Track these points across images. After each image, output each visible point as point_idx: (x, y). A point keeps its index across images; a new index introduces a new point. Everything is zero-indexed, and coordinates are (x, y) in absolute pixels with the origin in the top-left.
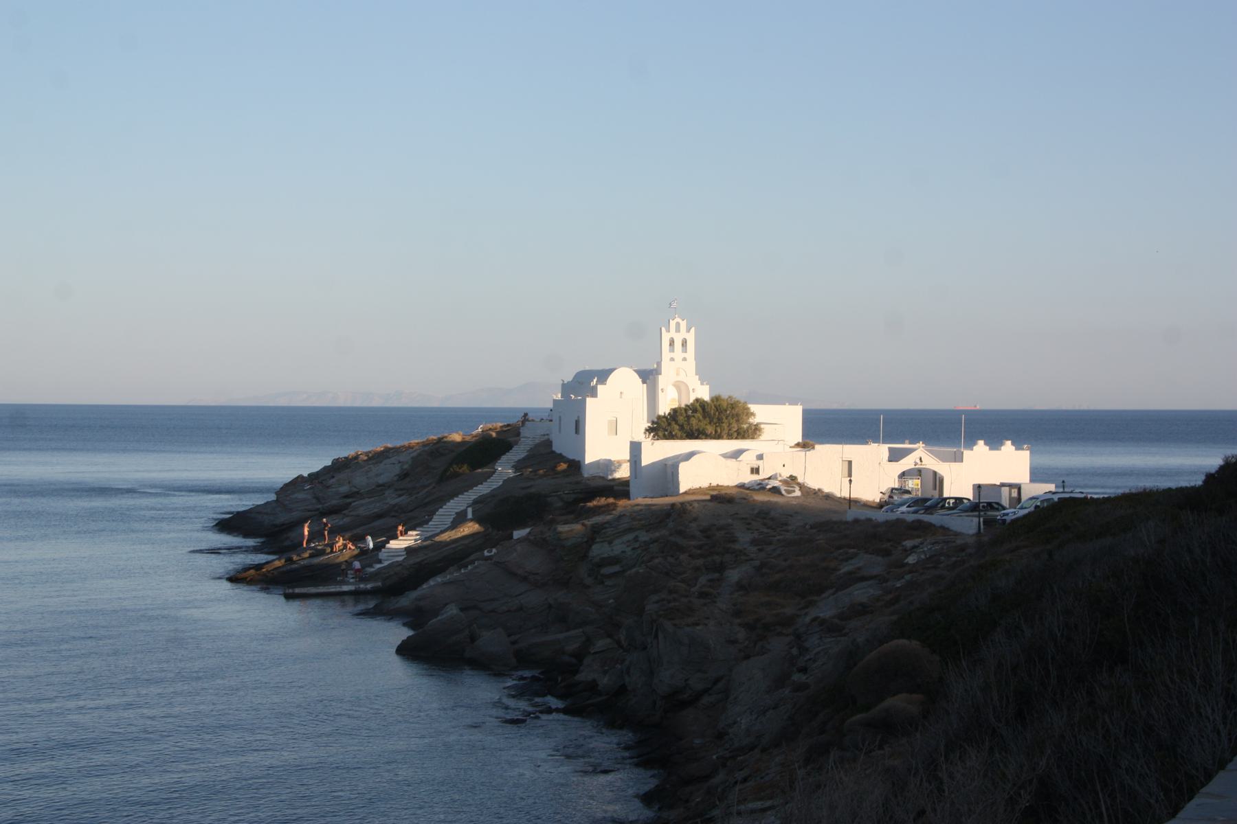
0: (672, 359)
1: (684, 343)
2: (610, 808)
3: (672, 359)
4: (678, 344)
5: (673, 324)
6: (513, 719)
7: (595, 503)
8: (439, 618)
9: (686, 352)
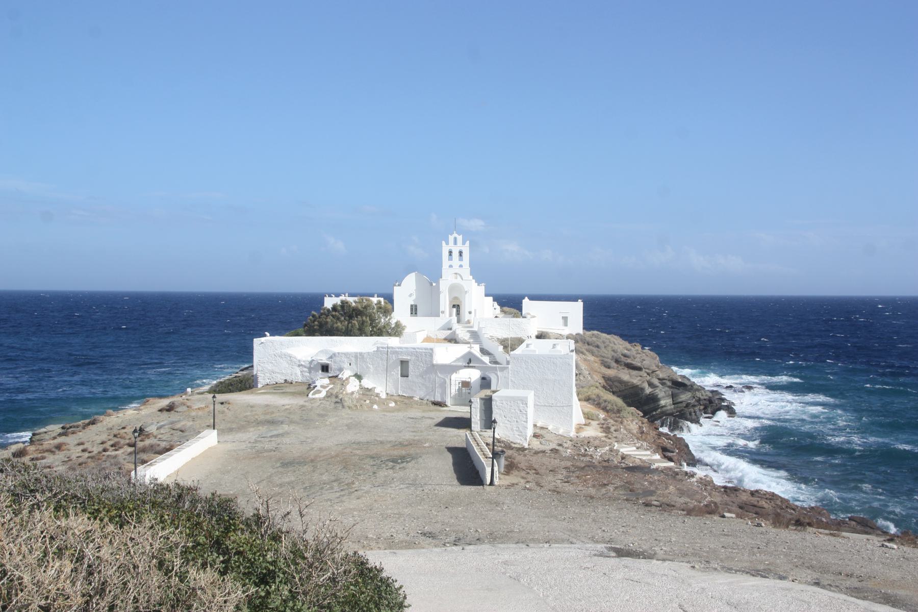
0: (451, 266)
1: (461, 253)
2: (43, 430)
4: (455, 254)
5: (451, 238)
6: (114, 411)
7: (686, 372)
8: (880, 440)
9: (452, 260)
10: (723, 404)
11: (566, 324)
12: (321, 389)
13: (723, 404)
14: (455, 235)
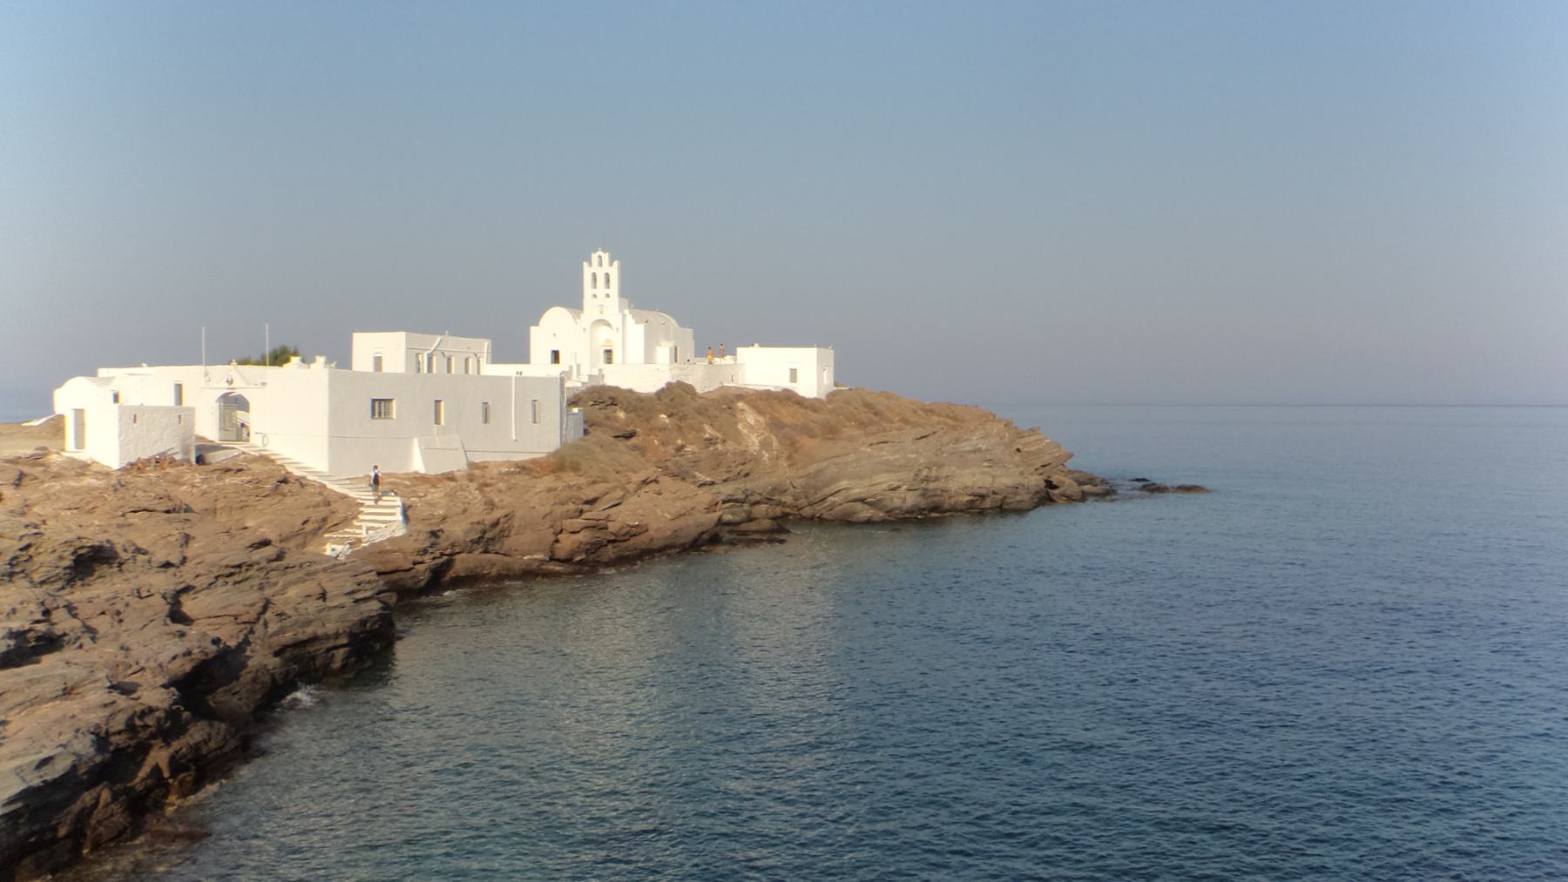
3: (595, 296)
5: (595, 257)
14: (600, 253)
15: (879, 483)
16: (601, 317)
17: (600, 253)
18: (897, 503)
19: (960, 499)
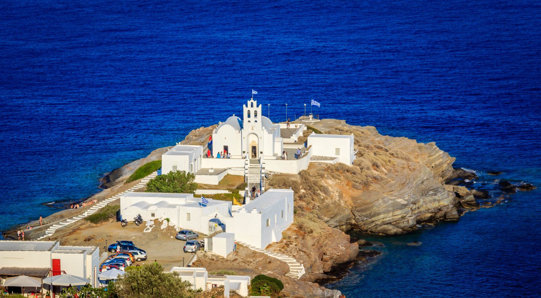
3: (249, 121)
4: (252, 114)
5: (249, 103)
10: (319, 104)
11: (189, 214)
12: (149, 228)
13: (319, 104)
14: (252, 101)
15: (397, 215)
16: (252, 132)
17: (252, 101)
18: (405, 224)
19: (426, 215)
